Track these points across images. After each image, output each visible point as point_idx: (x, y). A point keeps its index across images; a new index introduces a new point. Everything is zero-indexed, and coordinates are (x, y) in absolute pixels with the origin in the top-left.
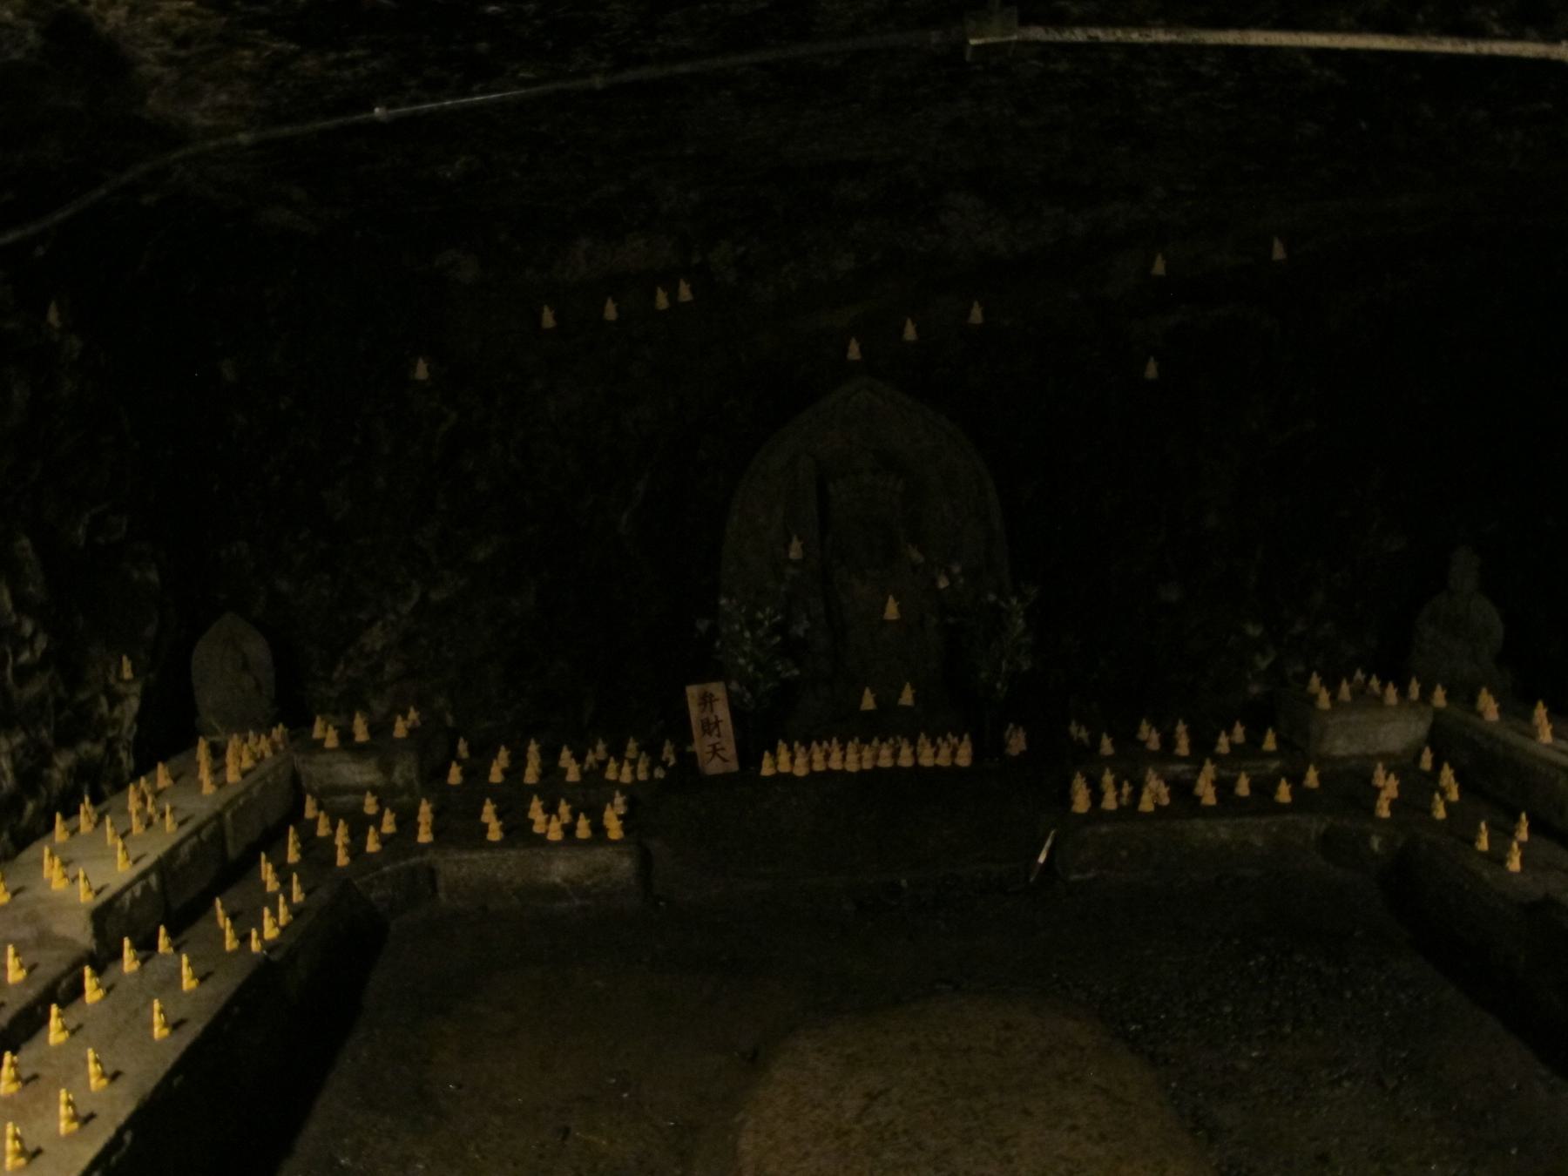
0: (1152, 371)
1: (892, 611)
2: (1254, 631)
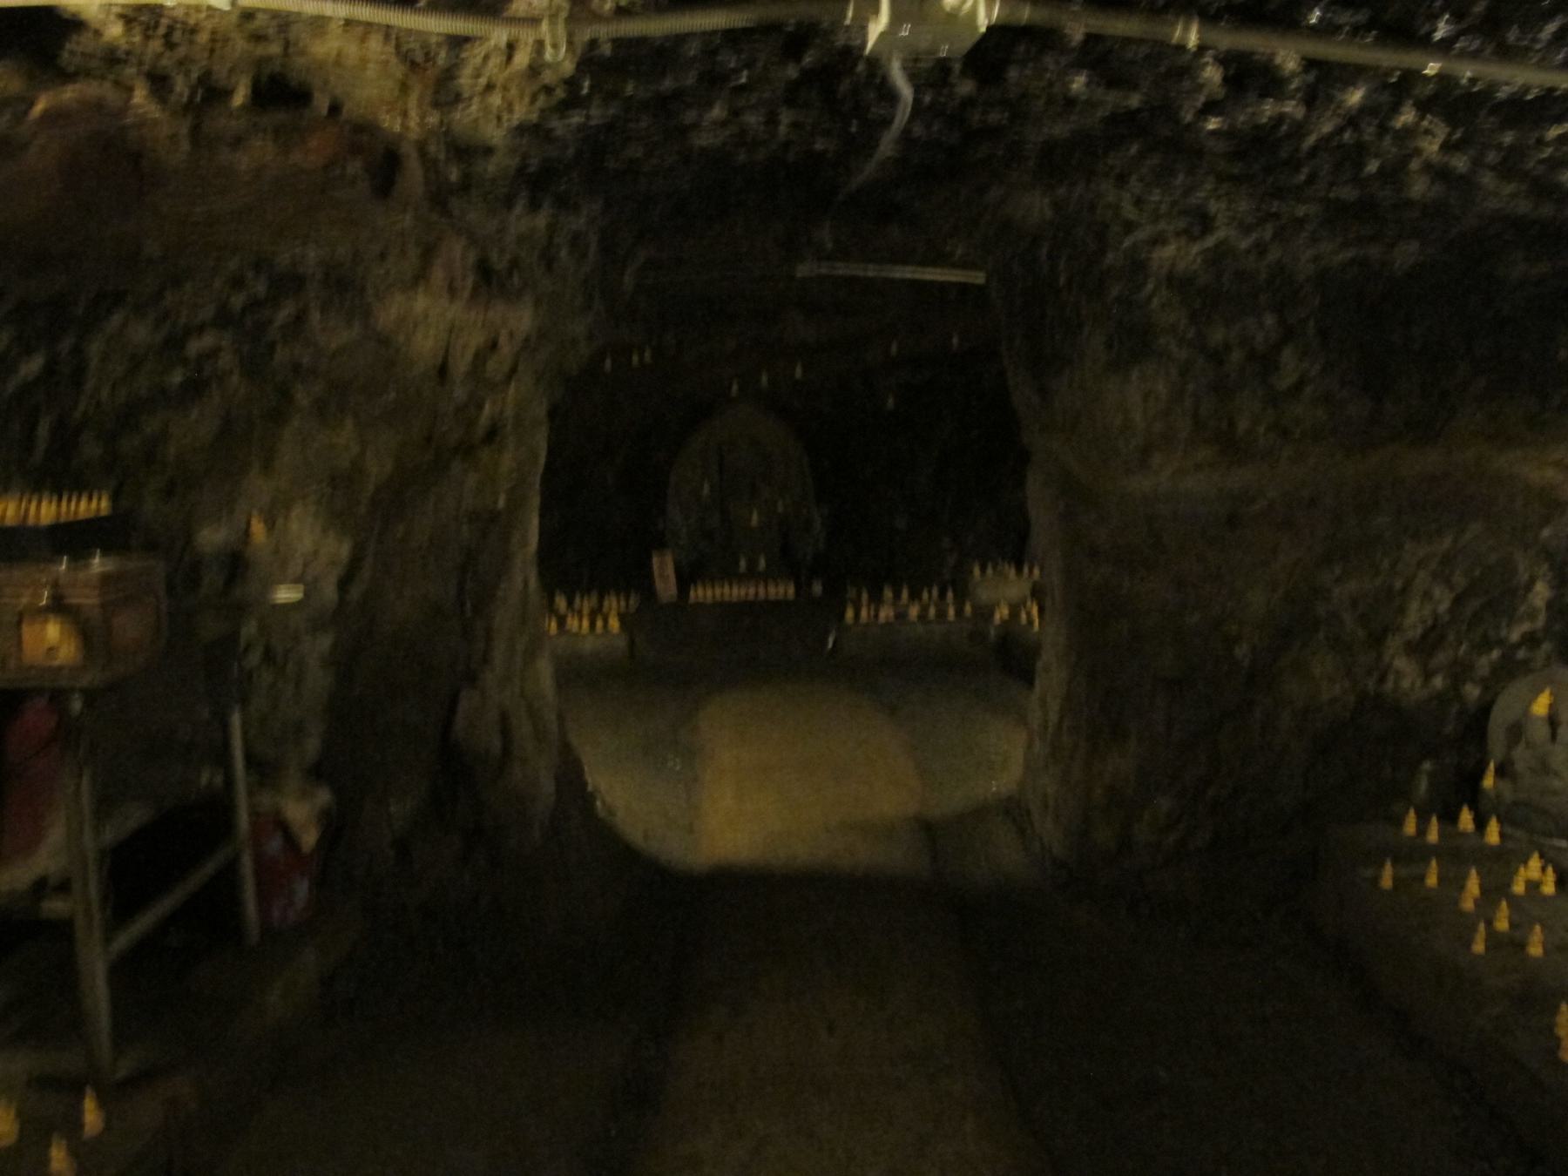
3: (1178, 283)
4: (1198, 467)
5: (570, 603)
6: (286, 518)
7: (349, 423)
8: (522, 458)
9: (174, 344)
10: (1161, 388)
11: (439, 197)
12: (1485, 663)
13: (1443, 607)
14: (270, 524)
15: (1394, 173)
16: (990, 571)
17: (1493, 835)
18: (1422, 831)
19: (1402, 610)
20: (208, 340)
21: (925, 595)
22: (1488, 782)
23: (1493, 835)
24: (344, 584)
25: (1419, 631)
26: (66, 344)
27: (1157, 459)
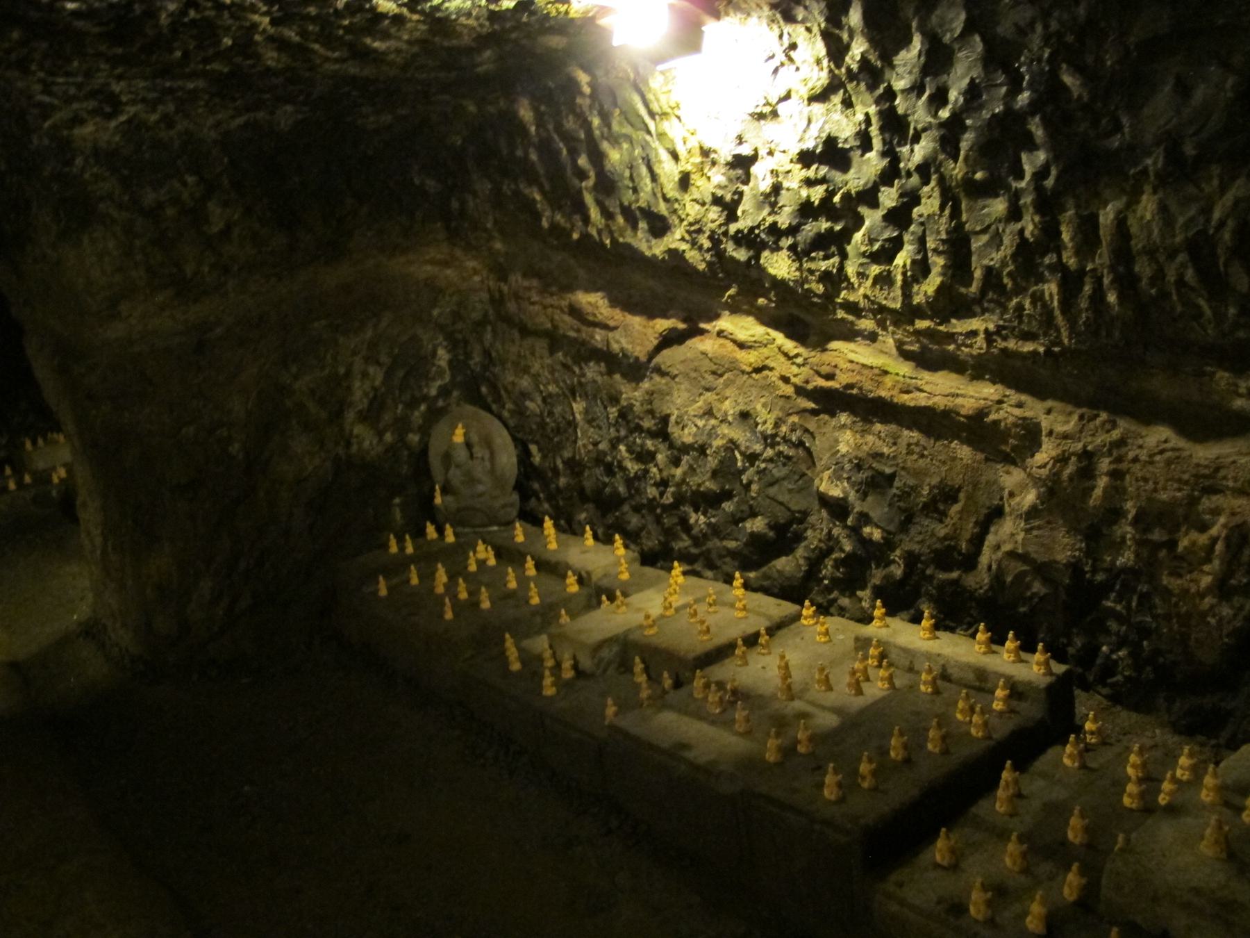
12: (417, 415)
15: (245, 45)
16: (40, 442)
17: (450, 538)
18: (402, 549)
19: (349, 388)
22: (438, 500)
23: (450, 538)
25: (366, 401)
27: (124, 307)
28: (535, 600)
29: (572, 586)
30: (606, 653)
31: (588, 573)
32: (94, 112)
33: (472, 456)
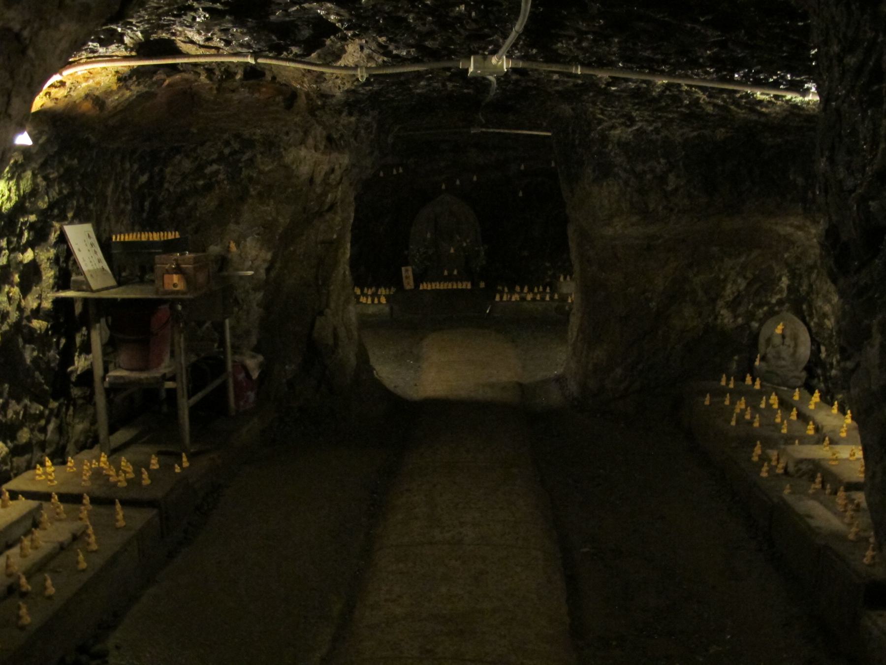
0: (521, 194)
1: (452, 251)
2: (548, 264)
3: (623, 145)
4: (633, 225)
5: (362, 291)
6: (245, 241)
7: (272, 202)
8: (342, 220)
9: (200, 168)
10: (616, 189)
11: (312, 110)
12: (760, 312)
13: (742, 288)
14: (238, 245)
16: (568, 278)
18: (727, 384)
19: (724, 288)
20: (215, 167)
21: (536, 290)
22: (757, 363)
23: (757, 386)
24: (268, 270)
25: (732, 297)
26: (156, 169)
28: (784, 431)
29: (810, 430)
30: (804, 467)
31: (823, 427)
32: (623, 124)
33: (783, 344)
